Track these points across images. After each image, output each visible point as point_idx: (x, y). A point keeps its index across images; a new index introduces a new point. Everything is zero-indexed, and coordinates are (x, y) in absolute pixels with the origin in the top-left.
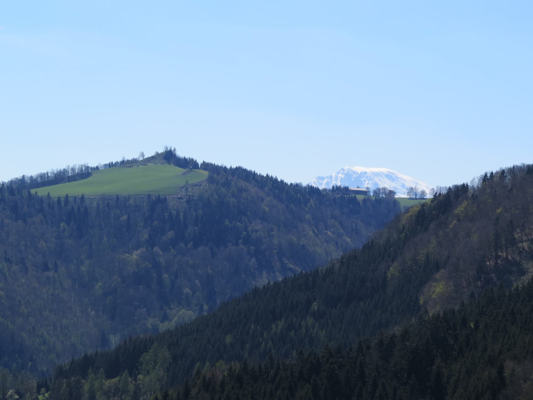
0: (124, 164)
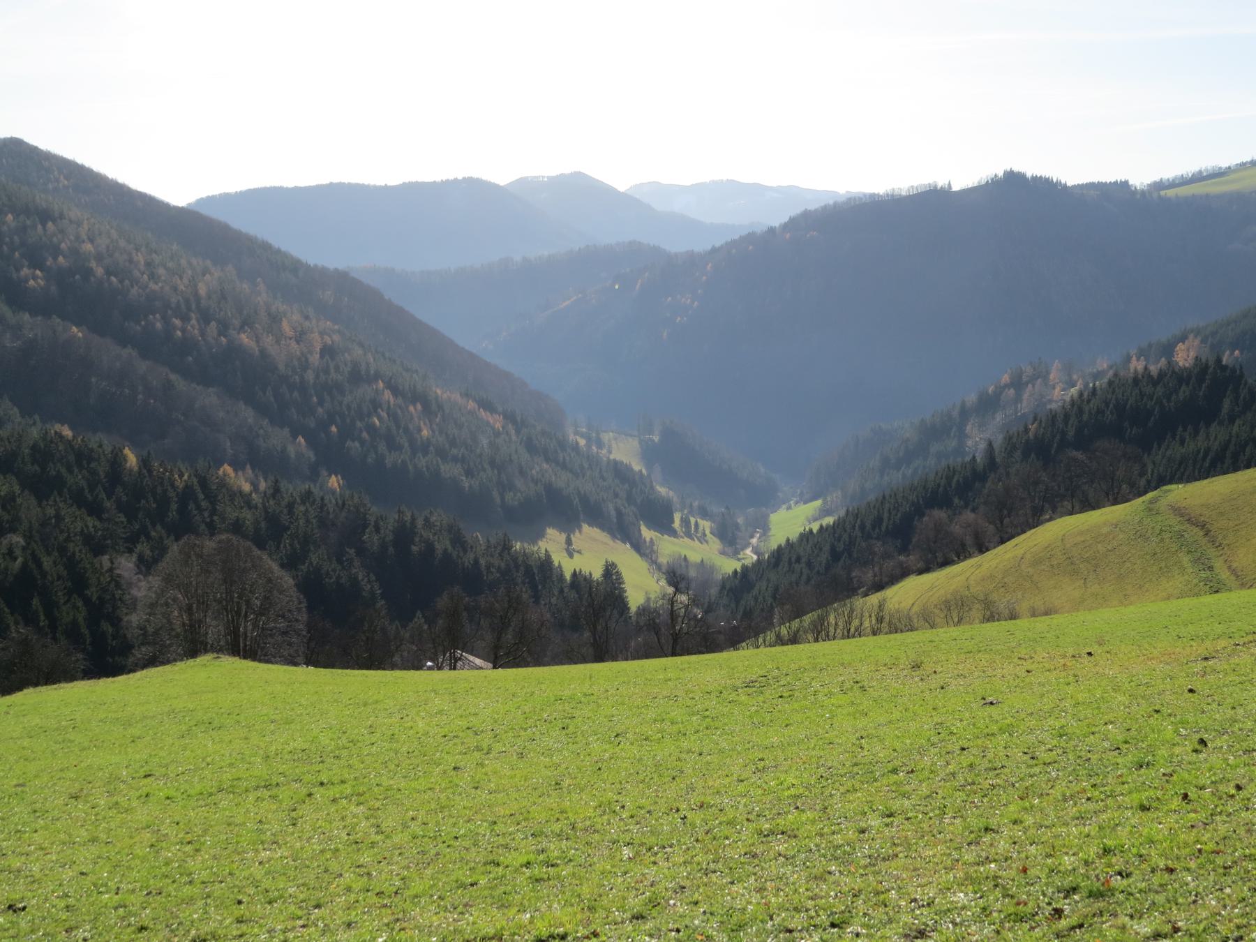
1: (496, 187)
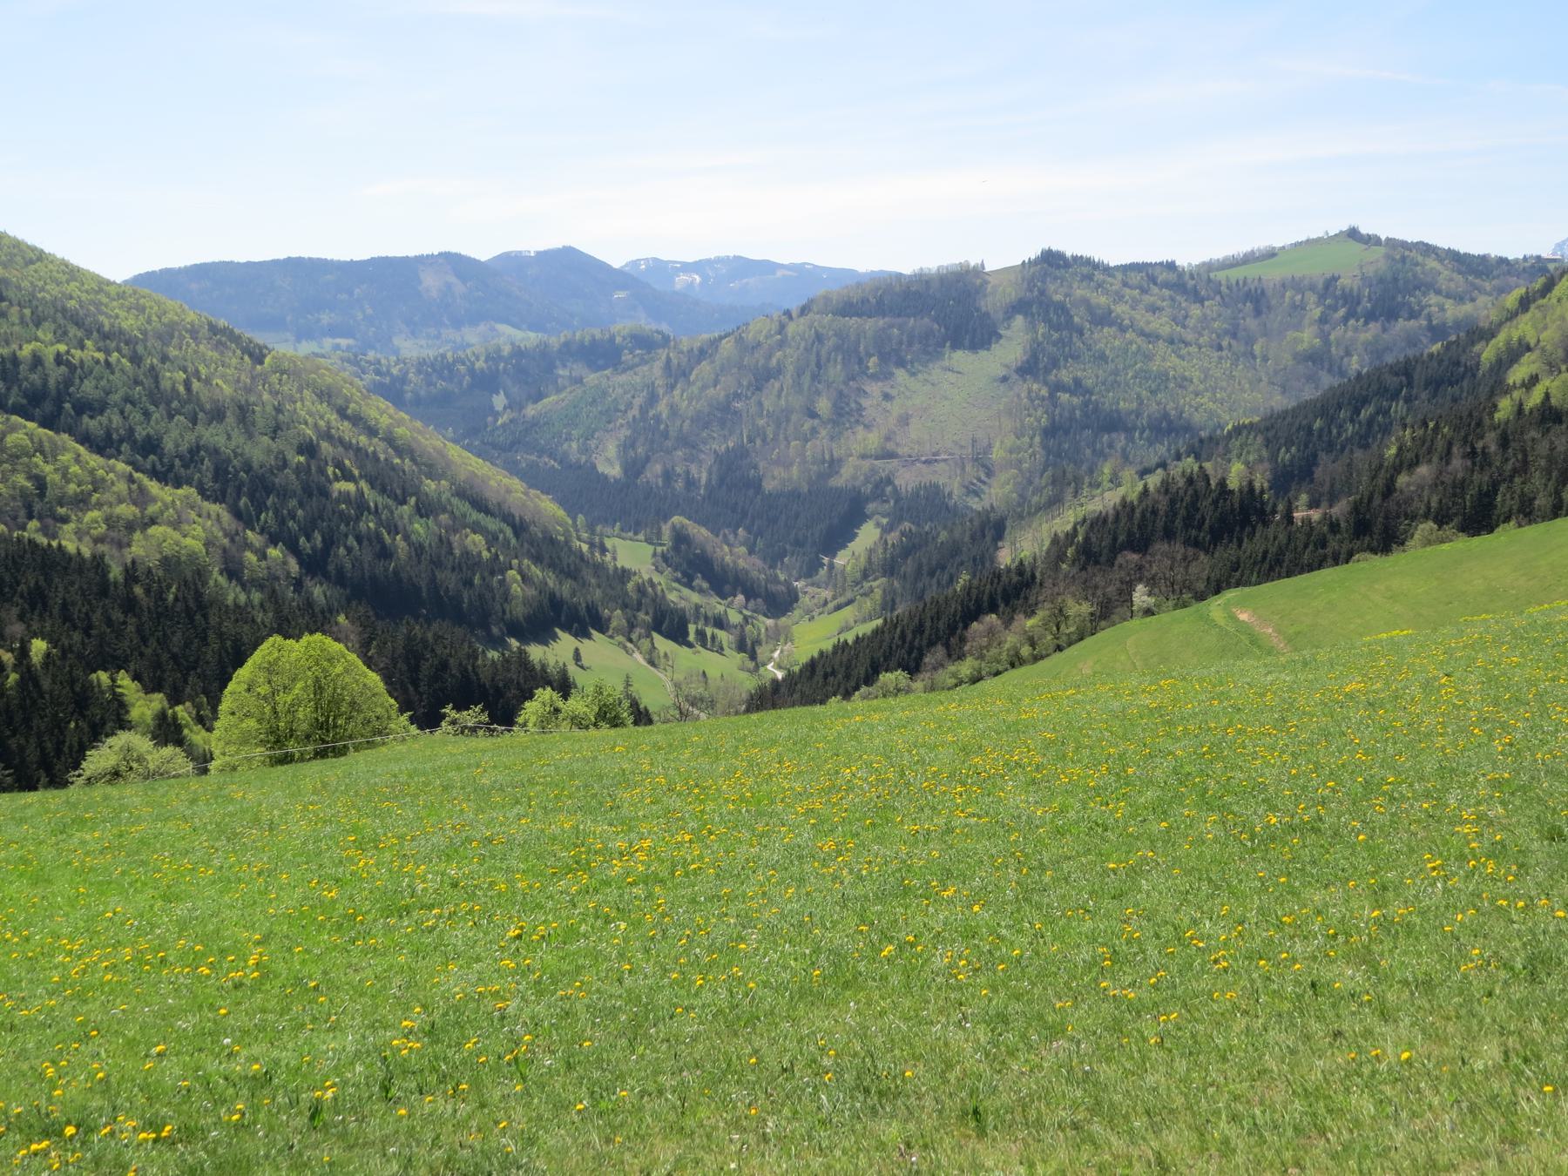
1: (478, 262)
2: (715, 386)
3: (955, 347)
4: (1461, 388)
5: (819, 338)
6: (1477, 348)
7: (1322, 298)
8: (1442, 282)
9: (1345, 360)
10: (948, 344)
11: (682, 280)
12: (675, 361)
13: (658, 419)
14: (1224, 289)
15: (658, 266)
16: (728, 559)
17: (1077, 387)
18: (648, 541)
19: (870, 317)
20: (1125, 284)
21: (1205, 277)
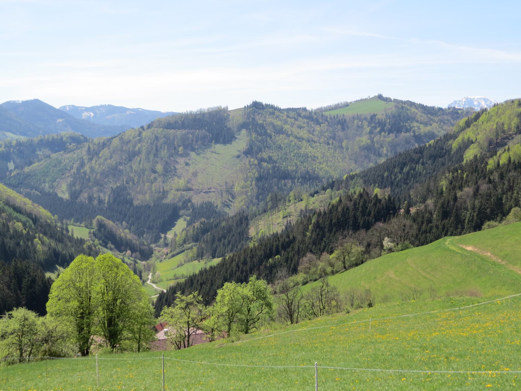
0: (361, 100)
2: (111, 159)
3: (217, 142)
4: (445, 159)
5: (157, 138)
6: (450, 142)
7: (370, 123)
8: (418, 118)
9: (381, 149)
10: (213, 141)
11: (85, 115)
12: (92, 148)
13: (85, 173)
14: (329, 119)
15: (74, 108)
16: (122, 235)
17: (270, 160)
18: (86, 227)
19: (179, 129)
20: (288, 117)
21: (321, 114)
